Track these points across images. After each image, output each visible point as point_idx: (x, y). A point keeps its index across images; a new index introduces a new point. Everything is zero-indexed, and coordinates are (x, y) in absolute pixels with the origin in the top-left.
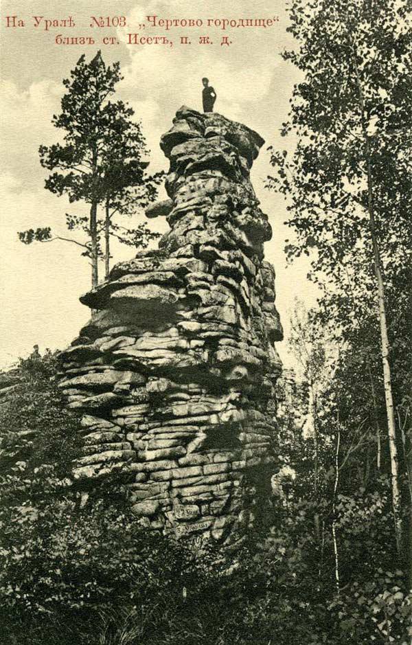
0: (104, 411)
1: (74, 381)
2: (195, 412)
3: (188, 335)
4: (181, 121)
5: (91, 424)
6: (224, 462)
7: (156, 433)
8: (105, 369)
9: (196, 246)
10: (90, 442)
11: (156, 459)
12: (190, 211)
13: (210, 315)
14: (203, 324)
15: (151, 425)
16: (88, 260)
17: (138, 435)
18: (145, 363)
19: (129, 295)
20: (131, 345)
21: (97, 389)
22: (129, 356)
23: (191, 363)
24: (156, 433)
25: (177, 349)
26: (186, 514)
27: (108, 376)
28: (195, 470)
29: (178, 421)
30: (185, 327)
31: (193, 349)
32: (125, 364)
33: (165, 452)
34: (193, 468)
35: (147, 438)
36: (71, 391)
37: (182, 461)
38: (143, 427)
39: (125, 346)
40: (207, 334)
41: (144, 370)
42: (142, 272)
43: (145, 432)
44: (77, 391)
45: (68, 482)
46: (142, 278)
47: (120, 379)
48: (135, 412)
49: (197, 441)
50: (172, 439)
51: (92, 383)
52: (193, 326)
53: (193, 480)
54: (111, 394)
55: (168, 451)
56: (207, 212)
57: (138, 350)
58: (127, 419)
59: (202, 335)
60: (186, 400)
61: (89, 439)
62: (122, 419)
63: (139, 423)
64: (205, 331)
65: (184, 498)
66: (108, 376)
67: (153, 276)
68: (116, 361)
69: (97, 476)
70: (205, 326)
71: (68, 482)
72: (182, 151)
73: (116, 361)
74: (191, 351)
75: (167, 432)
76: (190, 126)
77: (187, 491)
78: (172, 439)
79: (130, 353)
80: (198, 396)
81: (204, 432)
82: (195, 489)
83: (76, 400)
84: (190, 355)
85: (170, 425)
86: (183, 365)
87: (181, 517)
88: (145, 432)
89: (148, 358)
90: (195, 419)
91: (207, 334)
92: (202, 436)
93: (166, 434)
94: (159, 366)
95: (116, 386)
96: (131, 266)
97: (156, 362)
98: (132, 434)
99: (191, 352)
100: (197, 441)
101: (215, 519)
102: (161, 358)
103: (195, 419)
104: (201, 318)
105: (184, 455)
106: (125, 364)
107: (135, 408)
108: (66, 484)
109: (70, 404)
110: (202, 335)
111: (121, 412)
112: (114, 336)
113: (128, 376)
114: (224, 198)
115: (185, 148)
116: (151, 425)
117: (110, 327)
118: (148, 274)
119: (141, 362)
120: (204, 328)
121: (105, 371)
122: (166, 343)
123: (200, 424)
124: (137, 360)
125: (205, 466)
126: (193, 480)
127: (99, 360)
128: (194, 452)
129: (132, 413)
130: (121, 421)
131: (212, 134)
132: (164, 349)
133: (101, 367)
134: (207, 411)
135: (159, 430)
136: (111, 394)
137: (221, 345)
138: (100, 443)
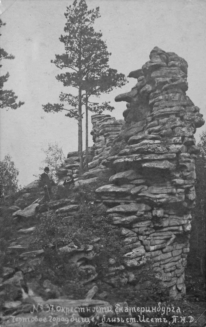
0: (129, 226)
1: (116, 209)
2: (172, 225)
3: (178, 186)
4: (157, 56)
5: (126, 233)
6: (180, 249)
7: (154, 236)
8: (131, 202)
9: (183, 137)
10: (127, 244)
11: (154, 251)
12: (173, 114)
13: (190, 176)
14: (186, 181)
15: (151, 232)
16: (74, 121)
17: (145, 237)
18: (155, 201)
19: (156, 166)
20: (146, 190)
21: (128, 214)
22: (147, 197)
23: (176, 201)
24: (154, 236)
25: (171, 194)
26: (168, 278)
27: (133, 207)
28: (169, 254)
29: (165, 229)
30: (177, 182)
31: (178, 193)
32: (142, 200)
33: (159, 246)
34: (168, 253)
35: (150, 239)
36: (114, 215)
37: (164, 250)
38: (147, 233)
39: (143, 191)
40: (187, 186)
41: (153, 205)
42: (162, 154)
43: (148, 235)
44: (117, 215)
45: (123, 267)
46: (162, 157)
47: (140, 208)
48: (144, 225)
49: (172, 239)
50: (163, 239)
51: (126, 211)
52: (180, 181)
53: (169, 260)
54: (135, 217)
55: (160, 245)
56: (183, 116)
57: (152, 194)
58: (140, 229)
59: (185, 186)
60: (166, 218)
61: (127, 242)
62: (137, 229)
63: (145, 231)
64: (186, 184)
65: (166, 270)
66: (133, 207)
67: (167, 156)
68: (138, 199)
69: (139, 265)
70: (186, 182)
71: (123, 267)
72: (159, 75)
73: (138, 199)
74: (177, 194)
75: (159, 236)
76: (161, 59)
77: (167, 266)
78: (163, 239)
79: (148, 195)
80: (173, 216)
81: (175, 234)
82: (170, 265)
83: (117, 220)
84: (176, 196)
85: (161, 232)
86: (172, 201)
87: (166, 280)
88: (148, 235)
89: (157, 198)
90: (172, 228)
91: (187, 186)
92: (174, 237)
93: (159, 237)
94: (162, 202)
95: (138, 212)
96: (156, 150)
97: (161, 201)
98: (142, 236)
99: (177, 195)
100: (172, 239)
101: (178, 279)
102: (163, 198)
103: (172, 228)
104: (184, 178)
105: (165, 248)
106: (142, 200)
107: (144, 223)
108: (122, 268)
109: (114, 222)
110: (185, 186)
111: (137, 225)
112: (137, 185)
113: (144, 207)
114: (193, 109)
115: (160, 73)
116: (151, 232)
117: (135, 179)
118: (165, 155)
119: (153, 200)
120: (186, 183)
121: (131, 203)
122: (165, 191)
123: (172, 231)
124: (151, 199)
125: (173, 252)
126: (169, 260)
127: (129, 197)
128: (169, 245)
129: (143, 226)
130: (136, 230)
131: (174, 65)
132: (165, 194)
133: (129, 201)
134: (178, 224)
135: (155, 234)
136: (135, 217)
137: (191, 191)
138: (131, 244)
